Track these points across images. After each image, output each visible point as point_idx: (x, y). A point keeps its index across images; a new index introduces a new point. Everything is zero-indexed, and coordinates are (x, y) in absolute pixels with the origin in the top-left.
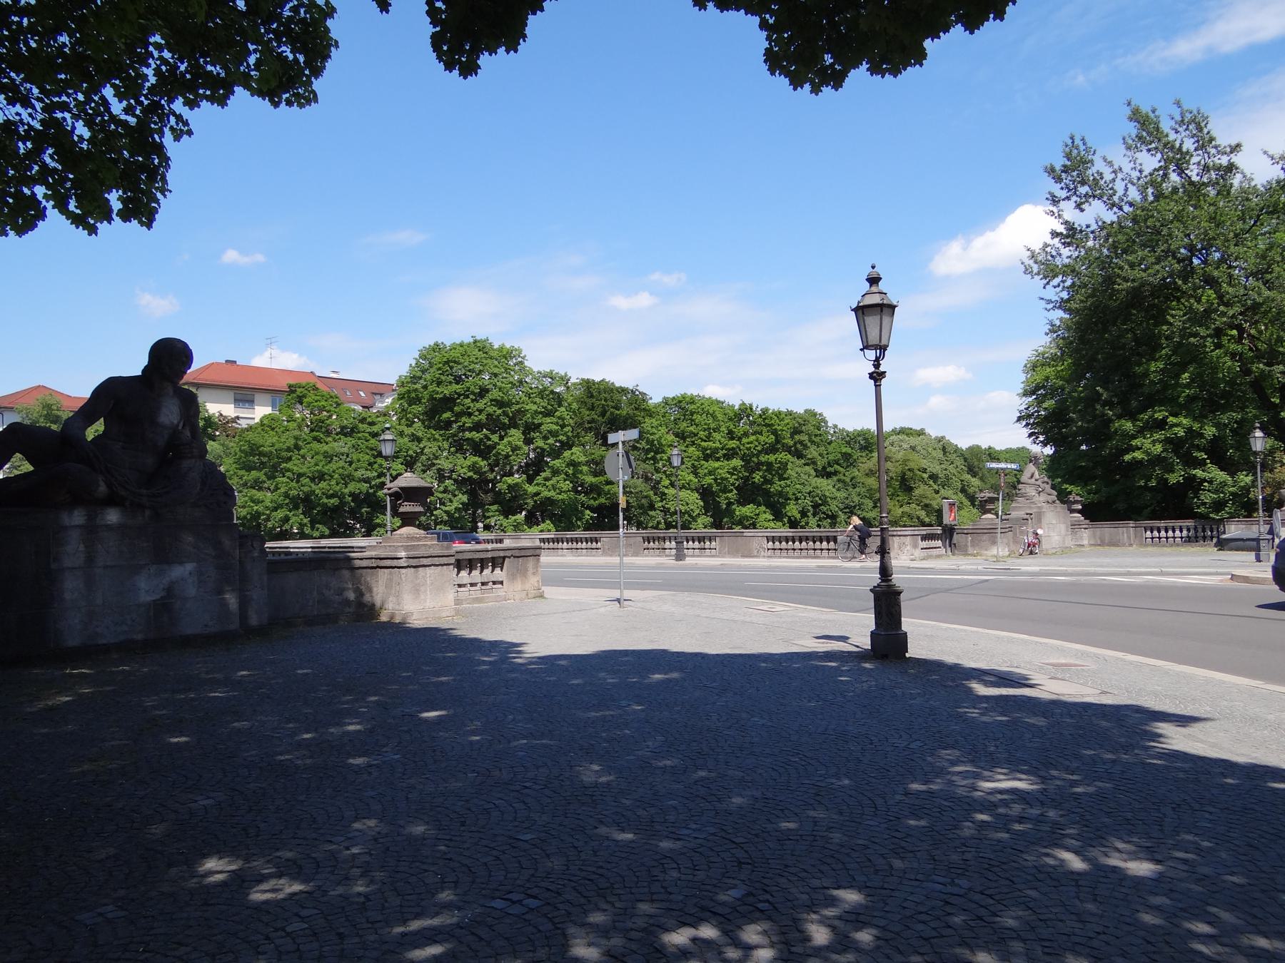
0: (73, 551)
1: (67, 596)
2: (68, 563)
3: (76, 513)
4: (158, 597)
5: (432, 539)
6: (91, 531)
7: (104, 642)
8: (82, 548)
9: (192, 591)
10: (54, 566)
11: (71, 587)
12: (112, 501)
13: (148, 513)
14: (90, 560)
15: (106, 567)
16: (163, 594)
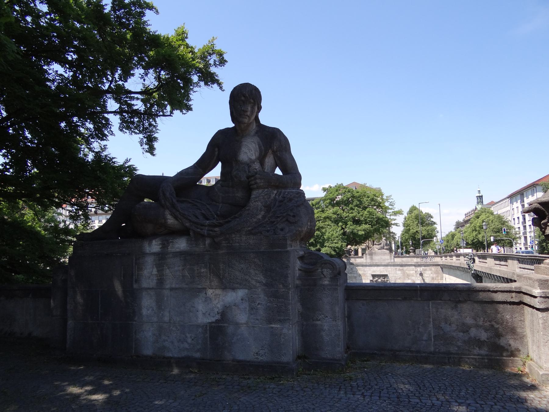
0: (149, 273)
1: (144, 312)
2: (145, 285)
3: (154, 242)
4: (213, 320)
5: (385, 254)
6: (161, 258)
7: (170, 355)
8: (155, 271)
9: (242, 317)
10: (135, 286)
11: (147, 304)
12: (183, 232)
13: (208, 241)
14: (161, 282)
15: (171, 289)
16: (218, 317)
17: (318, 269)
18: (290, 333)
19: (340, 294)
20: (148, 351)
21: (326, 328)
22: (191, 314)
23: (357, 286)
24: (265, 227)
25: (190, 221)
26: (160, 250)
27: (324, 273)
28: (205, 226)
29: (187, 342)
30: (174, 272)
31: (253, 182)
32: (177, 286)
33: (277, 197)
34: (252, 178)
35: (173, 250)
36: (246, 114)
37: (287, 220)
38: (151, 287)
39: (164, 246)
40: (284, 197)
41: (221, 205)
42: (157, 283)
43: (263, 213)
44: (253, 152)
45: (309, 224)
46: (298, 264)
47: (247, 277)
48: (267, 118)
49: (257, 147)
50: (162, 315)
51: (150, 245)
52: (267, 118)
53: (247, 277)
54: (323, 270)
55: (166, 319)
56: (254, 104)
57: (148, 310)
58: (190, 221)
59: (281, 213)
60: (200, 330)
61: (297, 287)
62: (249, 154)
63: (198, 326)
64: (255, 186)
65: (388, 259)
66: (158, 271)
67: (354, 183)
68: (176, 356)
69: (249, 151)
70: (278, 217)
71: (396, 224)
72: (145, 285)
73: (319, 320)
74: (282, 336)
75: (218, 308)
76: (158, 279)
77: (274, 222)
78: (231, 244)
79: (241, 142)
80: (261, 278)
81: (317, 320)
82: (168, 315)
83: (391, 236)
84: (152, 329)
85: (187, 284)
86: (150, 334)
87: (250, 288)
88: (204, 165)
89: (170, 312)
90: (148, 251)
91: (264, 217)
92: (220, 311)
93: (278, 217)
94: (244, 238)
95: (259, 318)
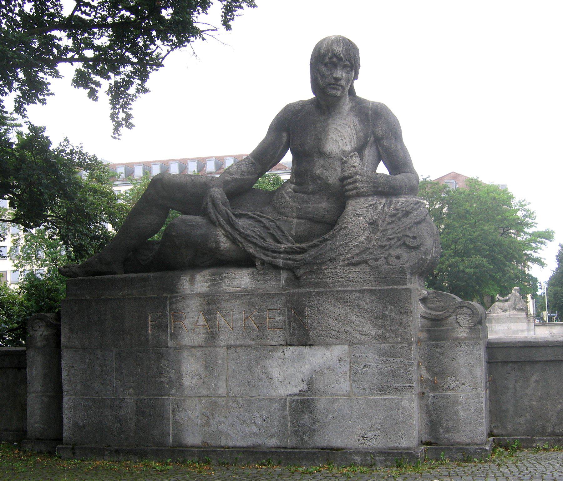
0: (191, 322)
1: (187, 381)
2: (186, 341)
4: (296, 390)
8: (202, 321)
12: (246, 262)
14: (212, 336)
15: (229, 347)
17: (450, 316)
18: (411, 406)
19: (481, 353)
20: (193, 439)
21: (462, 399)
22: (261, 383)
23: (505, 343)
24: (371, 253)
25: (255, 245)
26: (207, 289)
27: (459, 321)
28: (280, 253)
29: (255, 423)
30: (232, 323)
31: (350, 187)
32: (238, 342)
33: (386, 209)
34: (349, 181)
35: (230, 289)
36: (339, 83)
37: (404, 244)
38: (197, 344)
39: (215, 283)
40: (397, 210)
41: (295, 221)
42: (206, 338)
43: (367, 233)
44: (348, 139)
45: (434, 249)
46: (421, 309)
47: (347, 328)
48: (366, 87)
49: (354, 132)
50: (216, 385)
51: (192, 281)
52: (366, 87)
53: (347, 328)
54: (458, 316)
55: (222, 391)
56: (352, 70)
57: (192, 379)
58: (255, 245)
59: (394, 233)
60: (276, 406)
61: (419, 341)
62: (341, 143)
63: (272, 400)
64: (354, 192)
65: (522, 331)
66: (207, 321)
67: (453, 175)
68: (238, 444)
69: (341, 136)
70: (391, 239)
71: (538, 261)
72: (186, 341)
73: (453, 389)
74: (401, 411)
75: (303, 373)
76: (207, 333)
77: (385, 246)
78: (321, 279)
79: (328, 125)
80: (369, 329)
81: (449, 389)
82: (225, 385)
83: (529, 285)
84: (199, 406)
85: (253, 340)
86: (197, 413)
87: (351, 344)
88: (265, 157)
89: (227, 381)
90: (189, 292)
91: (369, 239)
92: (306, 378)
93: (391, 239)
94: (340, 271)
95: (366, 386)
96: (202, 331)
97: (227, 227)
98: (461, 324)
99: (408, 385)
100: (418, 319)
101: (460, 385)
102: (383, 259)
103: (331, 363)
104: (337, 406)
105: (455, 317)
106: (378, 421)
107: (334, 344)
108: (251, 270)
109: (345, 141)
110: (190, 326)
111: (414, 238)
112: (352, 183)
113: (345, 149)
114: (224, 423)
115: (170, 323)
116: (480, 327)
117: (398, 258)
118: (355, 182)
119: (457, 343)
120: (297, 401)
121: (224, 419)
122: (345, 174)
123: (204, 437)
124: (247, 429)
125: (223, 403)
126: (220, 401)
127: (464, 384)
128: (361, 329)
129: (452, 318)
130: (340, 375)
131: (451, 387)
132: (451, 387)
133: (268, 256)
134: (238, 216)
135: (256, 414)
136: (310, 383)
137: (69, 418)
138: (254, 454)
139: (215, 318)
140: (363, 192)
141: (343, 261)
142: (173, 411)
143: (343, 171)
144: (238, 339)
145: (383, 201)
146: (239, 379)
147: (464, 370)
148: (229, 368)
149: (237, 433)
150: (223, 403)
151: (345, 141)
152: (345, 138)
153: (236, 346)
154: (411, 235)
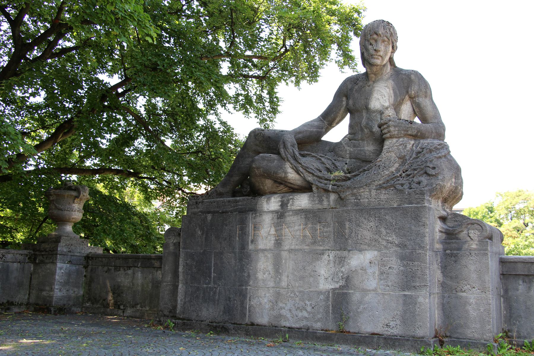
1: (260, 276)
8: (273, 231)
14: (278, 243)
19: (493, 266)
27: (471, 235)
32: (297, 247)
34: (385, 126)
35: (294, 208)
38: (268, 248)
42: (274, 243)
43: (397, 165)
44: (387, 97)
49: (392, 91)
54: (470, 231)
60: (322, 297)
62: (382, 101)
66: (276, 231)
72: (261, 246)
73: (464, 291)
78: (359, 200)
82: (286, 279)
85: (308, 245)
95: (390, 284)
96: (272, 239)
97: (292, 161)
98: (472, 237)
99: (424, 284)
100: (436, 233)
101: (470, 288)
102: (407, 184)
103: (364, 265)
104: (367, 299)
105: (467, 232)
106: (399, 313)
107: (366, 250)
108: (310, 193)
109: (385, 99)
110: (265, 234)
111: (434, 168)
112: (387, 128)
113: (384, 104)
114: (284, 309)
115: (251, 232)
116: (489, 241)
117: (419, 183)
118: (389, 126)
119: (468, 253)
120: (338, 294)
121: (284, 305)
122: (382, 122)
123: (270, 319)
124: (300, 314)
125: (285, 293)
126: (282, 291)
127: (474, 288)
128: (387, 238)
129: (464, 232)
130: (370, 274)
131: (463, 290)
132: (463, 290)
133: (321, 183)
134: (303, 156)
135: (307, 302)
136: (348, 279)
137: (181, 300)
138: (305, 335)
139: (282, 229)
140: (394, 135)
141: (377, 186)
142: (250, 298)
143: (381, 119)
144: (297, 245)
145: (412, 142)
146: (296, 275)
147: (474, 276)
148: (286, 262)
149: (292, 316)
150: (285, 293)
151: (385, 99)
152: (385, 97)
153: (296, 250)
154: (431, 166)
